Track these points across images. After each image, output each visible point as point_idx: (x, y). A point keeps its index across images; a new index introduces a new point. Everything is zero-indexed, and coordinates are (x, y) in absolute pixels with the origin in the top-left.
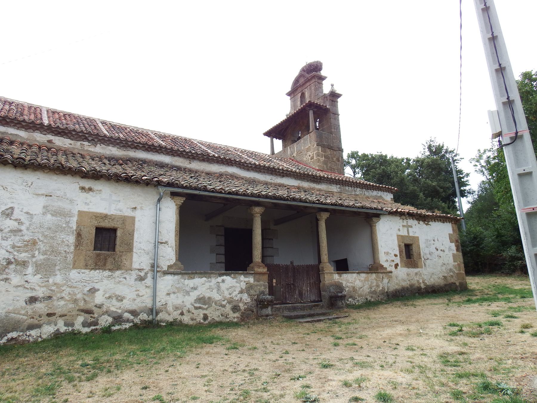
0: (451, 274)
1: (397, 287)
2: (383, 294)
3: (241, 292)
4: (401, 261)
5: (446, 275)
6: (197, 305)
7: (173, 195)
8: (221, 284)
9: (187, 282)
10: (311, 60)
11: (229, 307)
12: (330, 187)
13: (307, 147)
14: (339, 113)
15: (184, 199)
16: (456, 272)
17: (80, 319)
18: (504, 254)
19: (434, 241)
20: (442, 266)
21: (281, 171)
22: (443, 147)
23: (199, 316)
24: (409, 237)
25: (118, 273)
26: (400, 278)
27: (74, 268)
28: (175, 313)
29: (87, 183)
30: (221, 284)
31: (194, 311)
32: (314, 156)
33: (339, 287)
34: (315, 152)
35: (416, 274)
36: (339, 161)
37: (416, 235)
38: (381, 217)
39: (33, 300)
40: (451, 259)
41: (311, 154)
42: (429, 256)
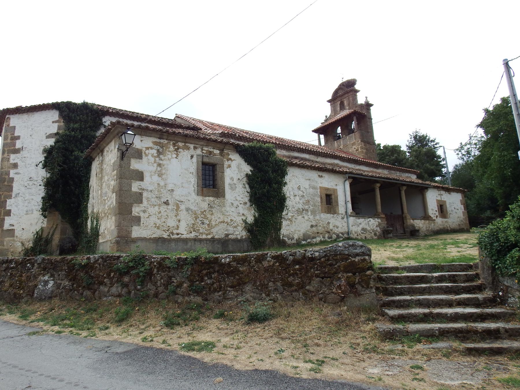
0: (462, 223)
1: (438, 228)
2: (432, 232)
3: (377, 226)
4: (439, 214)
5: (459, 223)
6: (362, 232)
7: (349, 178)
8: (369, 222)
9: (358, 220)
10: (347, 78)
11: (373, 233)
12: (384, 171)
13: (352, 142)
14: (372, 117)
15: (352, 180)
16: (465, 222)
17: (327, 235)
18: (482, 216)
19: (453, 203)
20: (457, 218)
21: (360, 162)
22: (427, 136)
23: (363, 236)
24: (441, 201)
25: (335, 215)
26: (439, 224)
27: (322, 213)
28: (355, 235)
29: (320, 173)
30: (369, 222)
31: (361, 234)
32: (358, 149)
33: (413, 226)
34: (359, 146)
35: (446, 222)
36: (374, 152)
37: (445, 200)
38: (429, 189)
39: (312, 226)
40: (462, 215)
41: (355, 147)
42: (451, 212)
